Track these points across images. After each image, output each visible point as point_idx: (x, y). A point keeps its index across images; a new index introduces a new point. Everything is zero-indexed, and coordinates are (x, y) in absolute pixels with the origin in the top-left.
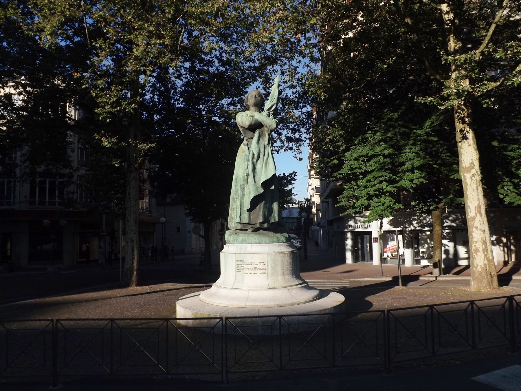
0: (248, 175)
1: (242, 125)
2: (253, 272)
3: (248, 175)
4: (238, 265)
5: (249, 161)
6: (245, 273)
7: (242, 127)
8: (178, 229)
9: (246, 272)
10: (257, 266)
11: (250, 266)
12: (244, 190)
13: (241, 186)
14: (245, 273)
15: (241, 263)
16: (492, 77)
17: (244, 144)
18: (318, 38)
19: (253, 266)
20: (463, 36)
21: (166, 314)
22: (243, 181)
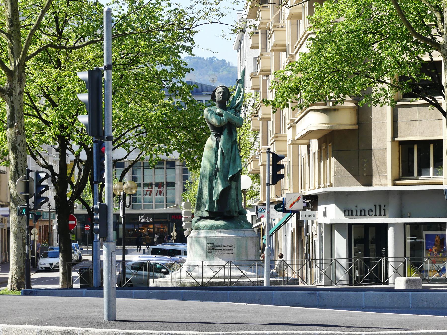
22: (212, 174)
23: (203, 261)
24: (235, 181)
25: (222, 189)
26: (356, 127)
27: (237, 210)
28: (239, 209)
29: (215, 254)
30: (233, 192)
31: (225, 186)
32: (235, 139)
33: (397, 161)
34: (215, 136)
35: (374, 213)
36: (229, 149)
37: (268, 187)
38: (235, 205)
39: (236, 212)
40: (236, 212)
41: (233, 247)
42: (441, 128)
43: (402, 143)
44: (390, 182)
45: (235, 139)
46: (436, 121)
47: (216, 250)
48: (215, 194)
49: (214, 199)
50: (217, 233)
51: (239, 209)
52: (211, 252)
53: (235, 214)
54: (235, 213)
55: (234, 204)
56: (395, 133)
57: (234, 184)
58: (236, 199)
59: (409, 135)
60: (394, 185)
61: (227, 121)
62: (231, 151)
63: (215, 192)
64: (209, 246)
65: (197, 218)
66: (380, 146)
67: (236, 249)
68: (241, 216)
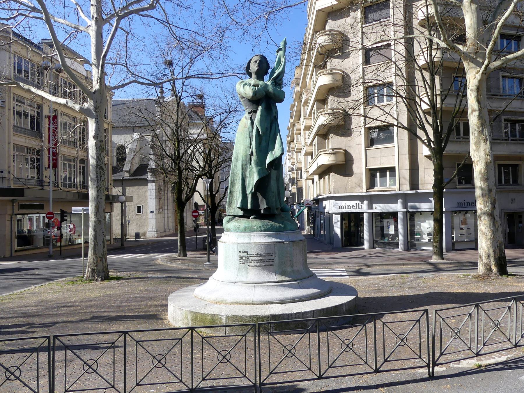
0: (252, 154)
4: (241, 257)
6: (249, 266)
8: (139, 209)
12: (246, 171)
13: (242, 166)
22: (246, 160)
23: (192, 329)
24: (275, 169)
25: (258, 179)
26: (344, 163)
27: (279, 206)
28: (281, 205)
29: (249, 266)
30: (273, 183)
31: (263, 175)
32: (275, 116)
33: (368, 180)
34: (250, 113)
35: (355, 207)
36: (267, 129)
37: (501, 41)
38: (276, 201)
39: (277, 209)
40: (277, 209)
41: (274, 256)
42: (394, 160)
43: (370, 170)
44: (365, 191)
45: (275, 116)
46: (391, 157)
47: (251, 261)
48: (249, 186)
49: (248, 192)
50: (207, 299)
51: (281, 205)
52: (244, 264)
53: (276, 212)
54: (276, 210)
55: (274, 199)
56: (366, 166)
57: (274, 173)
58: (277, 192)
59: (375, 165)
60: (367, 192)
61: (265, 93)
62: (269, 130)
63: (249, 184)
64: (242, 254)
65: (229, 217)
66: (359, 171)
67: (277, 258)
68: (283, 214)
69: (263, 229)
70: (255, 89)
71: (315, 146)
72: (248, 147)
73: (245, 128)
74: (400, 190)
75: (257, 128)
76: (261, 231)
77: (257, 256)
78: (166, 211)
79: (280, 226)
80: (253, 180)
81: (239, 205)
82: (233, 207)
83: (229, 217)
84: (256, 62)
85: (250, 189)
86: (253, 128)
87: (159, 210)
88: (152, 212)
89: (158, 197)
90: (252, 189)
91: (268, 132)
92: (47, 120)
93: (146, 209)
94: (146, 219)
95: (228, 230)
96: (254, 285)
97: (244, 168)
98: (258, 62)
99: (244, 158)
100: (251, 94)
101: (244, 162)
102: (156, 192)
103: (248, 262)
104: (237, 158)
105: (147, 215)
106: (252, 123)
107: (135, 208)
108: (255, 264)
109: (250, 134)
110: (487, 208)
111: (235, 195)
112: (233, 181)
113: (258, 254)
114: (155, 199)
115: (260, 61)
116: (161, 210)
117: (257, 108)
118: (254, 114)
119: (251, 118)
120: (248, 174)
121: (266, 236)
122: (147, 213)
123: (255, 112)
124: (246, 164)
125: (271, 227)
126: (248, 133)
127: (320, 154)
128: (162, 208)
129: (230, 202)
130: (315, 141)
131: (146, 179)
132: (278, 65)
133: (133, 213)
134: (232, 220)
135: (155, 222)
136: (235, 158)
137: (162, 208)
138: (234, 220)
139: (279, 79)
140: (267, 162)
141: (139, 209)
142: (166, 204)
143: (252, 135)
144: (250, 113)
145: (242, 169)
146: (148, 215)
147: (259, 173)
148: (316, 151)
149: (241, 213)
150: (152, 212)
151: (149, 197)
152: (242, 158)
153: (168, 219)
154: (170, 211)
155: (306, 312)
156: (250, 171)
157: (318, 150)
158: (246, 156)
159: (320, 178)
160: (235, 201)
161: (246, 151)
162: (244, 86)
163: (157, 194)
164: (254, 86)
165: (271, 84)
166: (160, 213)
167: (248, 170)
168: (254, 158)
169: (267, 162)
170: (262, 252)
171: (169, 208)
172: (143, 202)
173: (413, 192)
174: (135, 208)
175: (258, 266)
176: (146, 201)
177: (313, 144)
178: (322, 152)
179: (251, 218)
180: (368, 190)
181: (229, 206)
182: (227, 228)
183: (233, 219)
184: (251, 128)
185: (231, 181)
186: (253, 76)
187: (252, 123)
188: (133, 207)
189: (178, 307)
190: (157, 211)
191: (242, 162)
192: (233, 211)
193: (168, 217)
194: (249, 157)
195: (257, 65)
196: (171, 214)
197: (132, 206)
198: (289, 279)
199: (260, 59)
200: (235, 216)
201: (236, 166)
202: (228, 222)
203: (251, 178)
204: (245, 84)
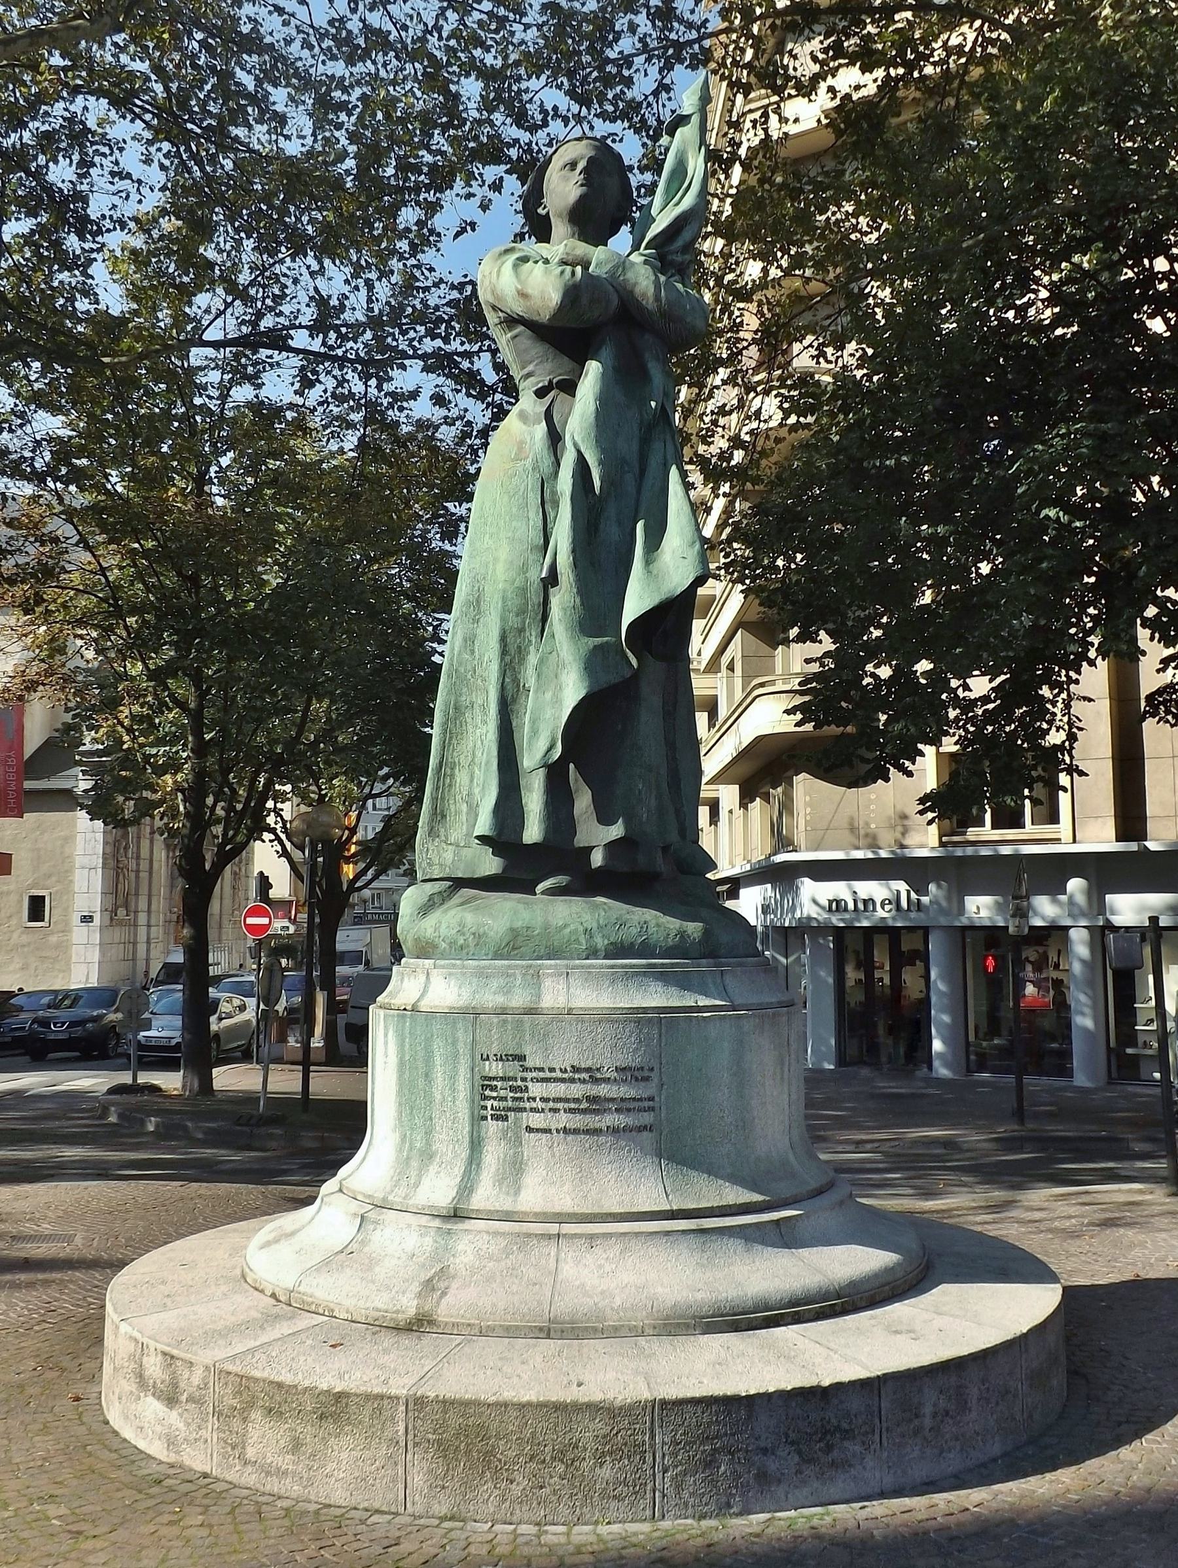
0: (552, 579)
1: (517, 307)
2: (577, 1121)
3: (552, 579)
4: (487, 1083)
5: (556, 504)
6: (530, 1130)
7: (511, 321)
8: (37, 908)
9: (536, 1120)
10: (603, 1090)
11: (559, 1090)
12: (522, 660)
13: (503, 639)
14: (530, 1130)
15: (513, 1068)
16: (1056, 888)
17: (523, 416)
18: (421, 153)
19: (577, 1090)
20: (895, 562)
21: (363, 1099)
22: (521, 612)
34: (541, 393)
48: (535, 732)
52: (505, 1119)
54: (659, 855)
63: (534, 721)
64: (495, 1068)
65: (430, 888)
69: (600, 942)
70: (573, 273)
71: (731, 668)
72: (533, 548)
73: (517, 458)
74: (1074, 841)
75: (580, 454)
76: (592, 953)
77: (572, 1081)
78: (142, 918)
79: (682, 934)
80: (557, 701)
81: (484, 824)
82: (452, 840)
83: (430, 888)
84: (573, 165)
85: (542, 745)
86: (558, 463)
87: (114, 912)
88: (88, 919)
89: (112, 863)
90: (551, 747)
91: (630, 480)
92: (83, 967)
93: (66, 909)
94: (64, 948)
95: (426, 950)
96: (554, 1228)
97: (512, 649)
98: (581, 165)
99: (514, 602)
100: (555, 297)
101: (514, 621)
102: (105, 843)
103: (524, 1110)
104: (476, 603)
105: (66, 930)
106: (555, 438)
107: (21, 901)
108: (563, 1120)
109: (546, 485)
110: (726, 1044)
111: (461, 777)
112: (457, 711)
113: (575, 1069)
114: (100, 871)
115: (591, 160)
116: (121, 912)
117: (579, 373)
118: (563, 395)
119: (548, 415)
120: (529, 677)
121: (632, 975)
122: (67, 923)
123: (569, 387)
124: (521, 631)
125: (640, 934)
126: (532, 483)
127: (756, 692)
128: (126, 906)
129: (439, 815)
130: (735, 649)
131: (68, 792)
132: (675, 185)
133: (14, 922)
134: (443, 902)
135: (96, 959)
136: (468, 604)
137: (126, 906)
138: (457, 899)
139: (679, 243)
140: (627, 619)
141: (37, 908)
142: (144, 890)
143: (554, 493)
144: (541, 393)
145: (504, 652)
146: (70, 931)
147: (593, 664)
148: (738, 682)
149: (490, 864)
150: (88, 919)
151: (78, 861)
152: (504, 599)
153: (148, 950)
154: (159, 918)
155: (838, 1387)
156: (542, 661)
157: (746, 678)
158: (523, 591)
159: (746, 798)
160: (464, 807)
161: (524, 569)
162: (515, 266)
163: (109, 849)
164: (563, 262)
165: (646, 262)
166: (121, 923)
167: (532, 659)
168: (562, 600)
169: (627, 619)
170: (607, 1059)
171: (154, 907)
172: (54, 879)
173: (1133, 846)
174: (21, 901)
175: (576, 1131)
176: (65, 876)
177: (725, 660)
178: (762, 685)
179: (540, 888)
180: (944, 839)
181: (432, 833)
182: (417, 940)
183: (450, 897)
184: (547, 462)
185: (446, 714)
186: (560, 228)
187: (555, 438)
188: (13, 898)
189: (152, 1344)
190: (107, 915)
191: (503, 619)
192: (449, 855)
193: (148, 942)
194: (535, 598)
195: (577, 176)
196: (161, 930)
197: (9, 893)
198: (757, 1197)
199: (592, 153)
200: (459, 883)
201: (470, 641)
202: (427, 908)
203: (548, 695)
204: (524, 259)
